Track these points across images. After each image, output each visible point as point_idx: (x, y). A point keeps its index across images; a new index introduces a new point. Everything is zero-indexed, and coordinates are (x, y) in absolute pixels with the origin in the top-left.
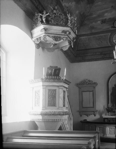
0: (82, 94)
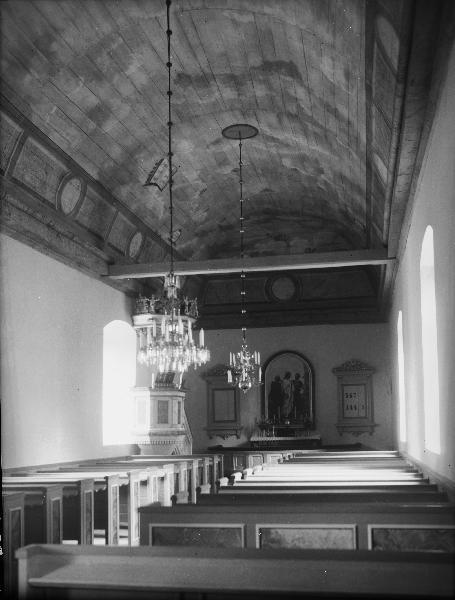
0: (213, 395)
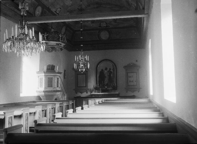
0: (77, 77)
